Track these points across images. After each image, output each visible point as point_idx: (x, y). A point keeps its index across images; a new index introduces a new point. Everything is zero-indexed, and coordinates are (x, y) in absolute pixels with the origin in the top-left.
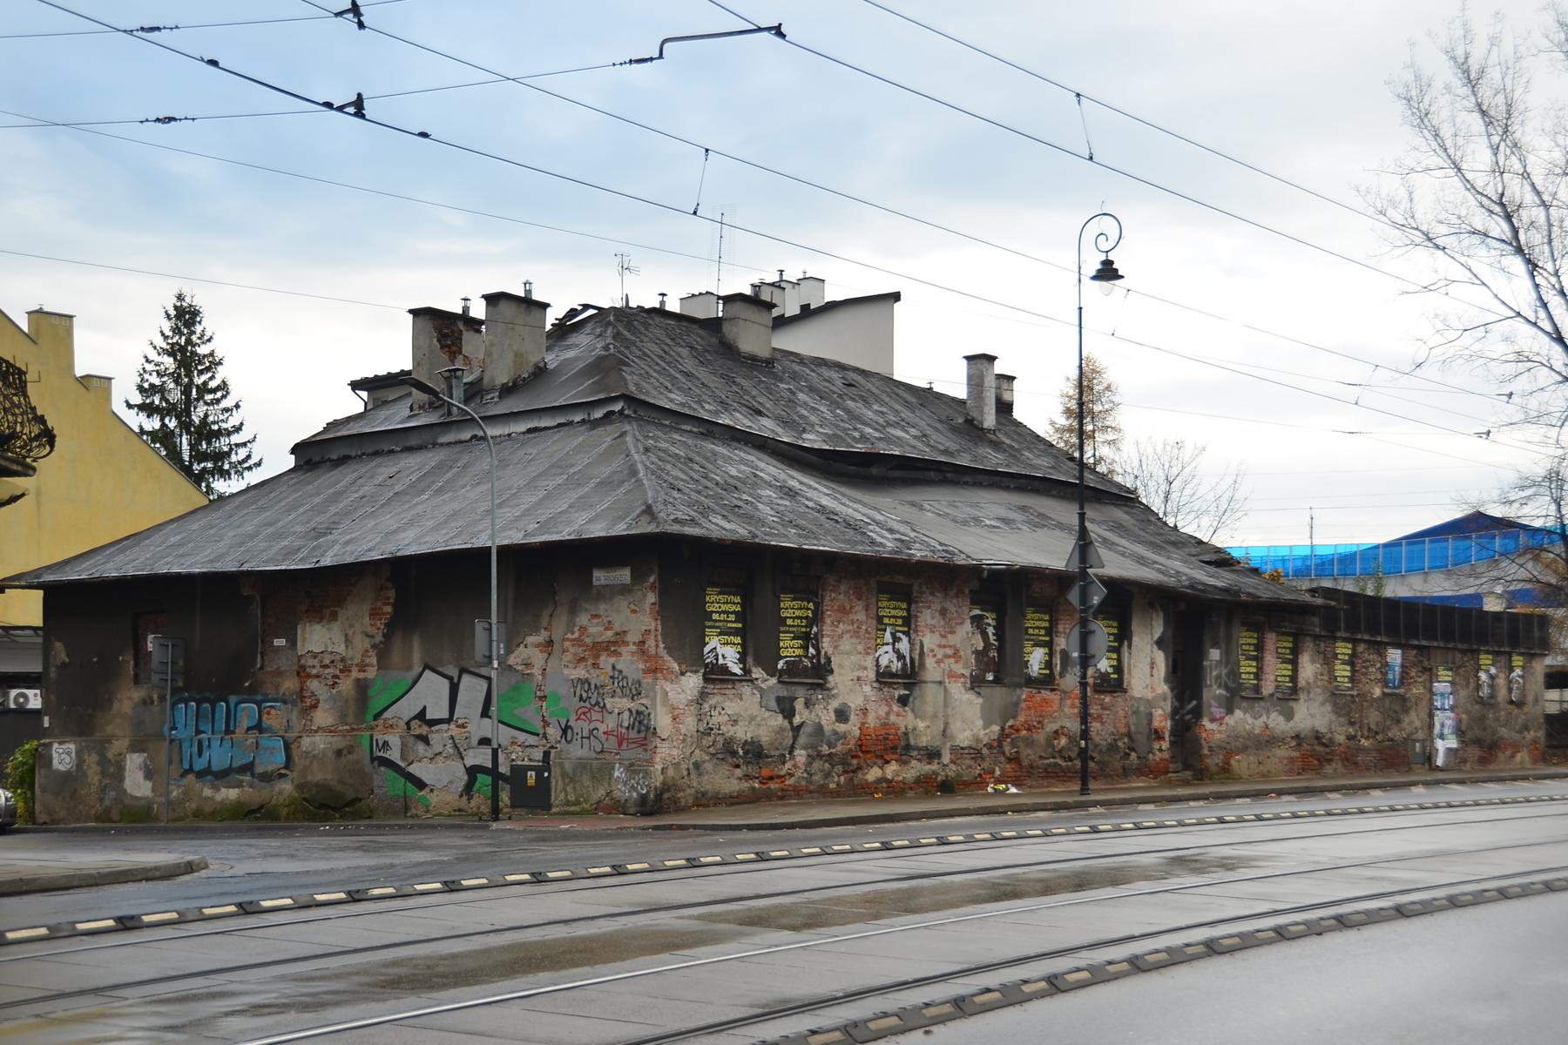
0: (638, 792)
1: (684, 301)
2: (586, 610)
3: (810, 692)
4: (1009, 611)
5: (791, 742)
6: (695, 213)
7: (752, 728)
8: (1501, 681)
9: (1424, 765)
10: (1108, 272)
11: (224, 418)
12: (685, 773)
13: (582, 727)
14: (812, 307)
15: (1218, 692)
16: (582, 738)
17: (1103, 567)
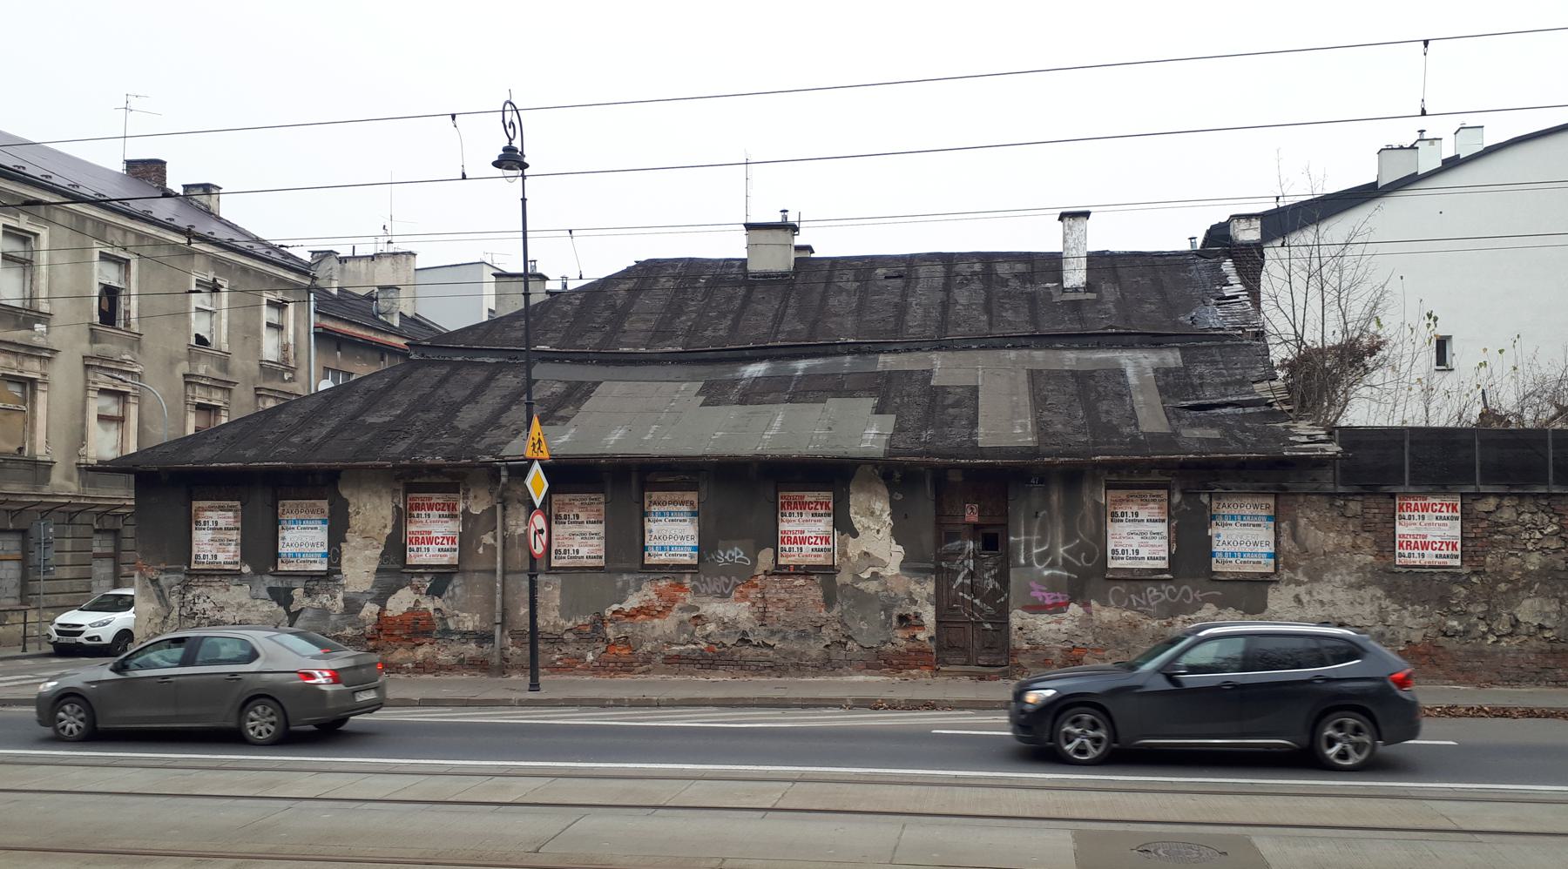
1: (762, 235)
7: (240, 613)
8: (1388, 550)
11: (1127, 361)
14: (1461, 157)
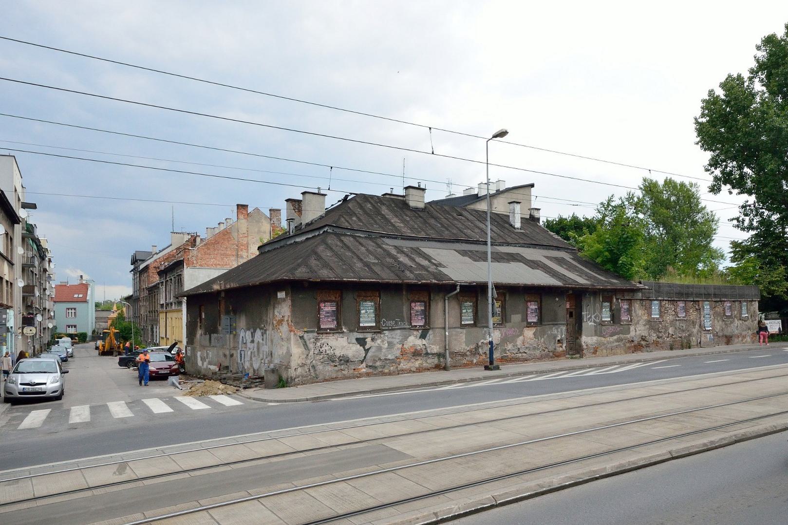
4: (479, 299)
5: (364, 355)
6: (329, 189)
12: (307, 370)
15: (590, 324)
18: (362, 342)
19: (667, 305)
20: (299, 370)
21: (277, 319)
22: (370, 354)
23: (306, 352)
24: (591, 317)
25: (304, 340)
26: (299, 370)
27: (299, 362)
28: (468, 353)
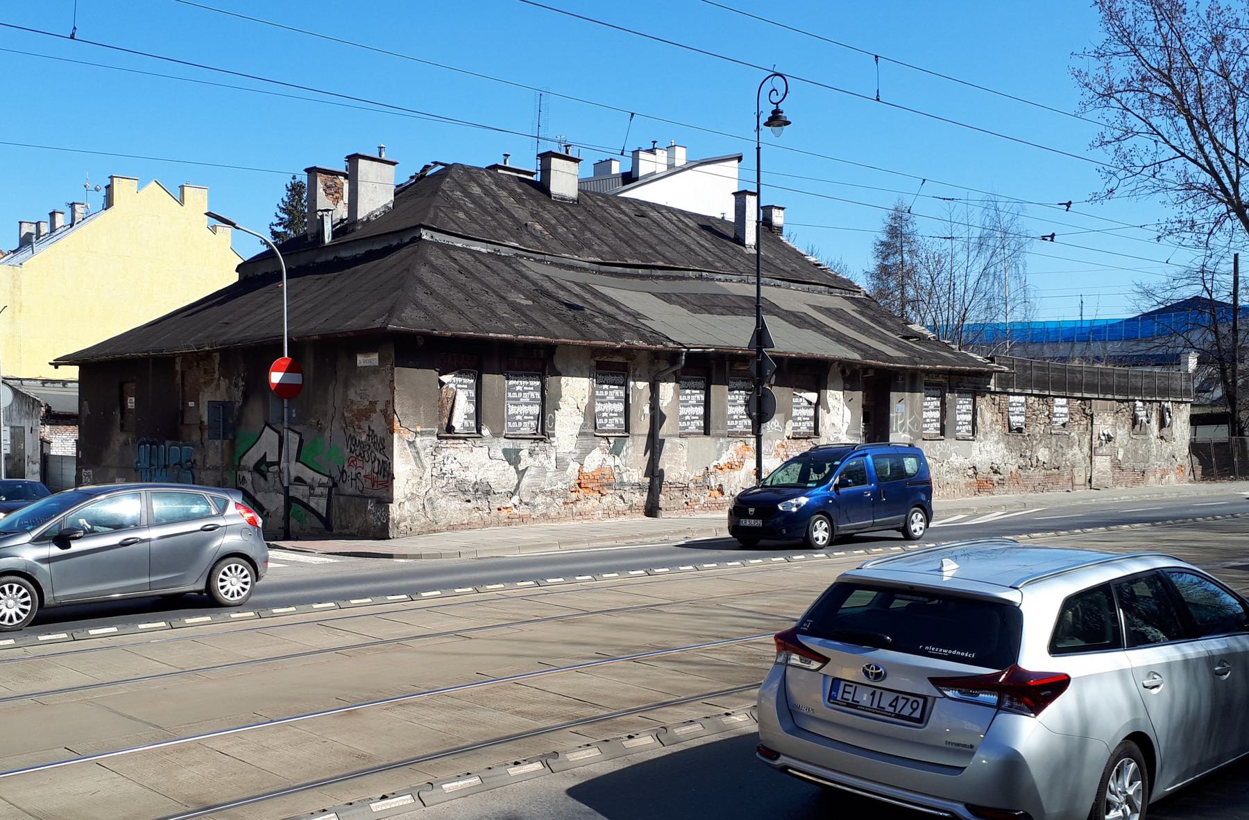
0: (381, 522)
2: (354, 385)
3: (533, 445)
5: (517, 482)
6: (72, 37)
9: (1085, 485)
10: (776, 119)
12: (421, 507)
13: (351, 471)
15: (903, 436)
16: (352, 479)
17: (773, 347)
18: (512, 457)
19: (1036, 405)
20: (407, 505)
21: (355, 407)
22: (526, 480)
23: (418, 473)
24: (903, 424)
25: (415, 448)
26: (407, 505)
27: (407, 491)
28: (692, 485)
